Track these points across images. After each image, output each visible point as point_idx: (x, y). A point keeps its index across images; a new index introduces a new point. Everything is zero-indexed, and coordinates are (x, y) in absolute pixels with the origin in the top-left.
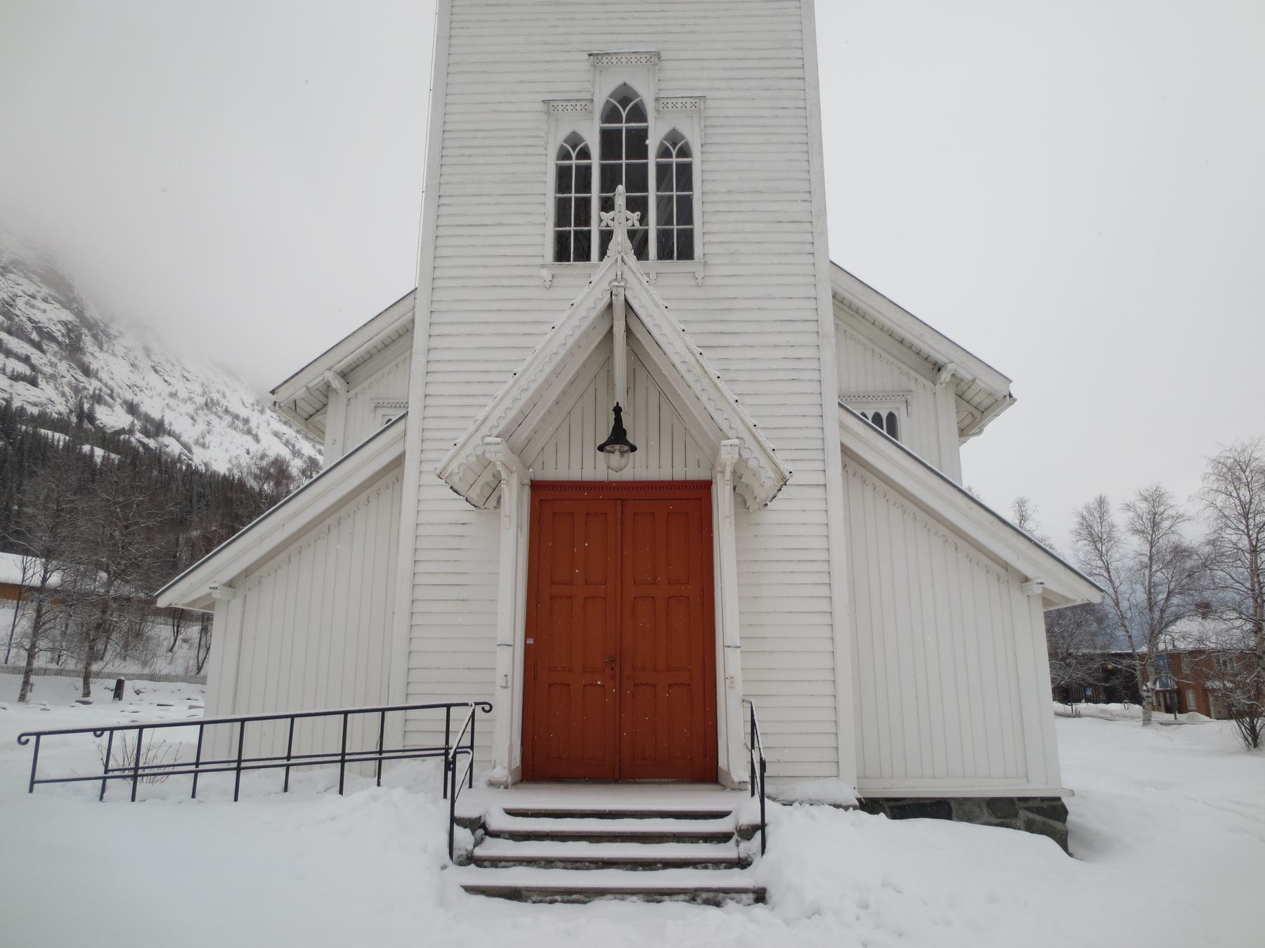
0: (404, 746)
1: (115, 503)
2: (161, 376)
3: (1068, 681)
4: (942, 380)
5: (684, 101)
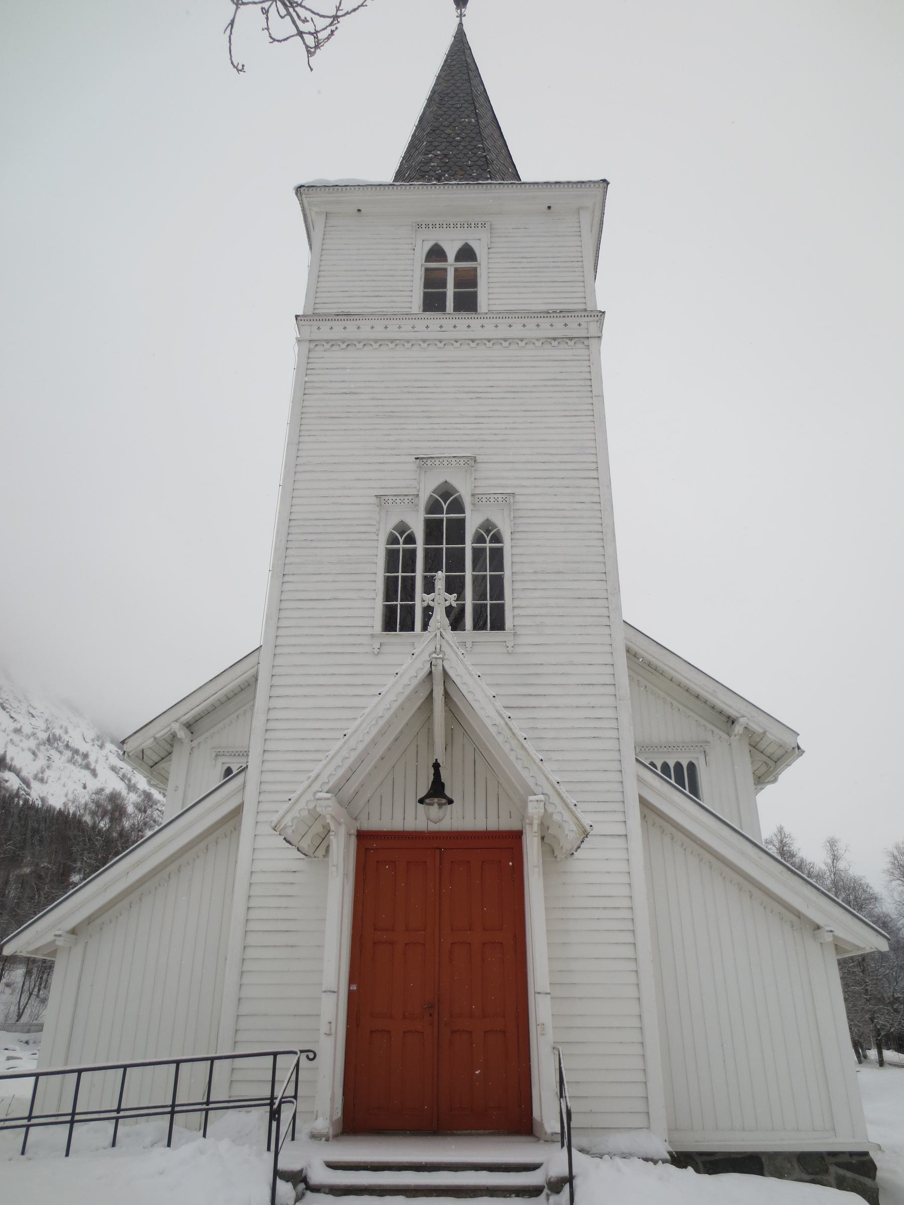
0: (230, 1097)
2: (7, 712)
3: (897, 1028)
4: (736, 732)
5: (496, 496)
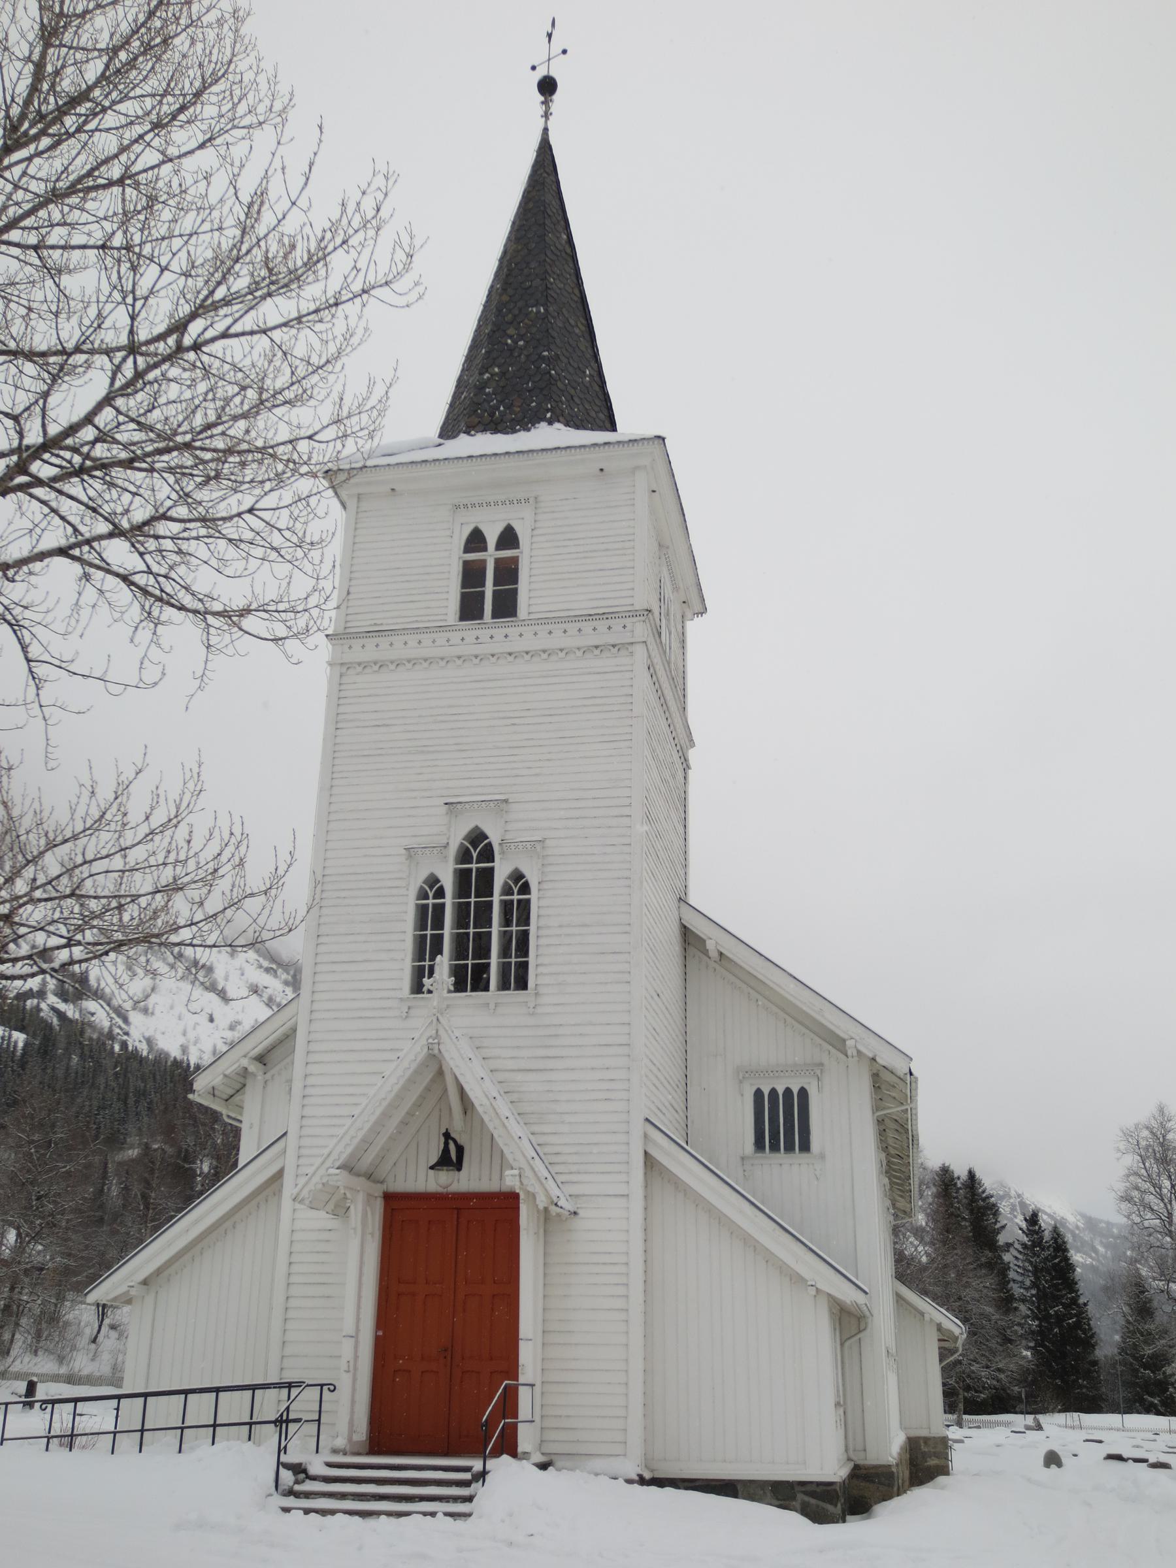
5: (524, 844)
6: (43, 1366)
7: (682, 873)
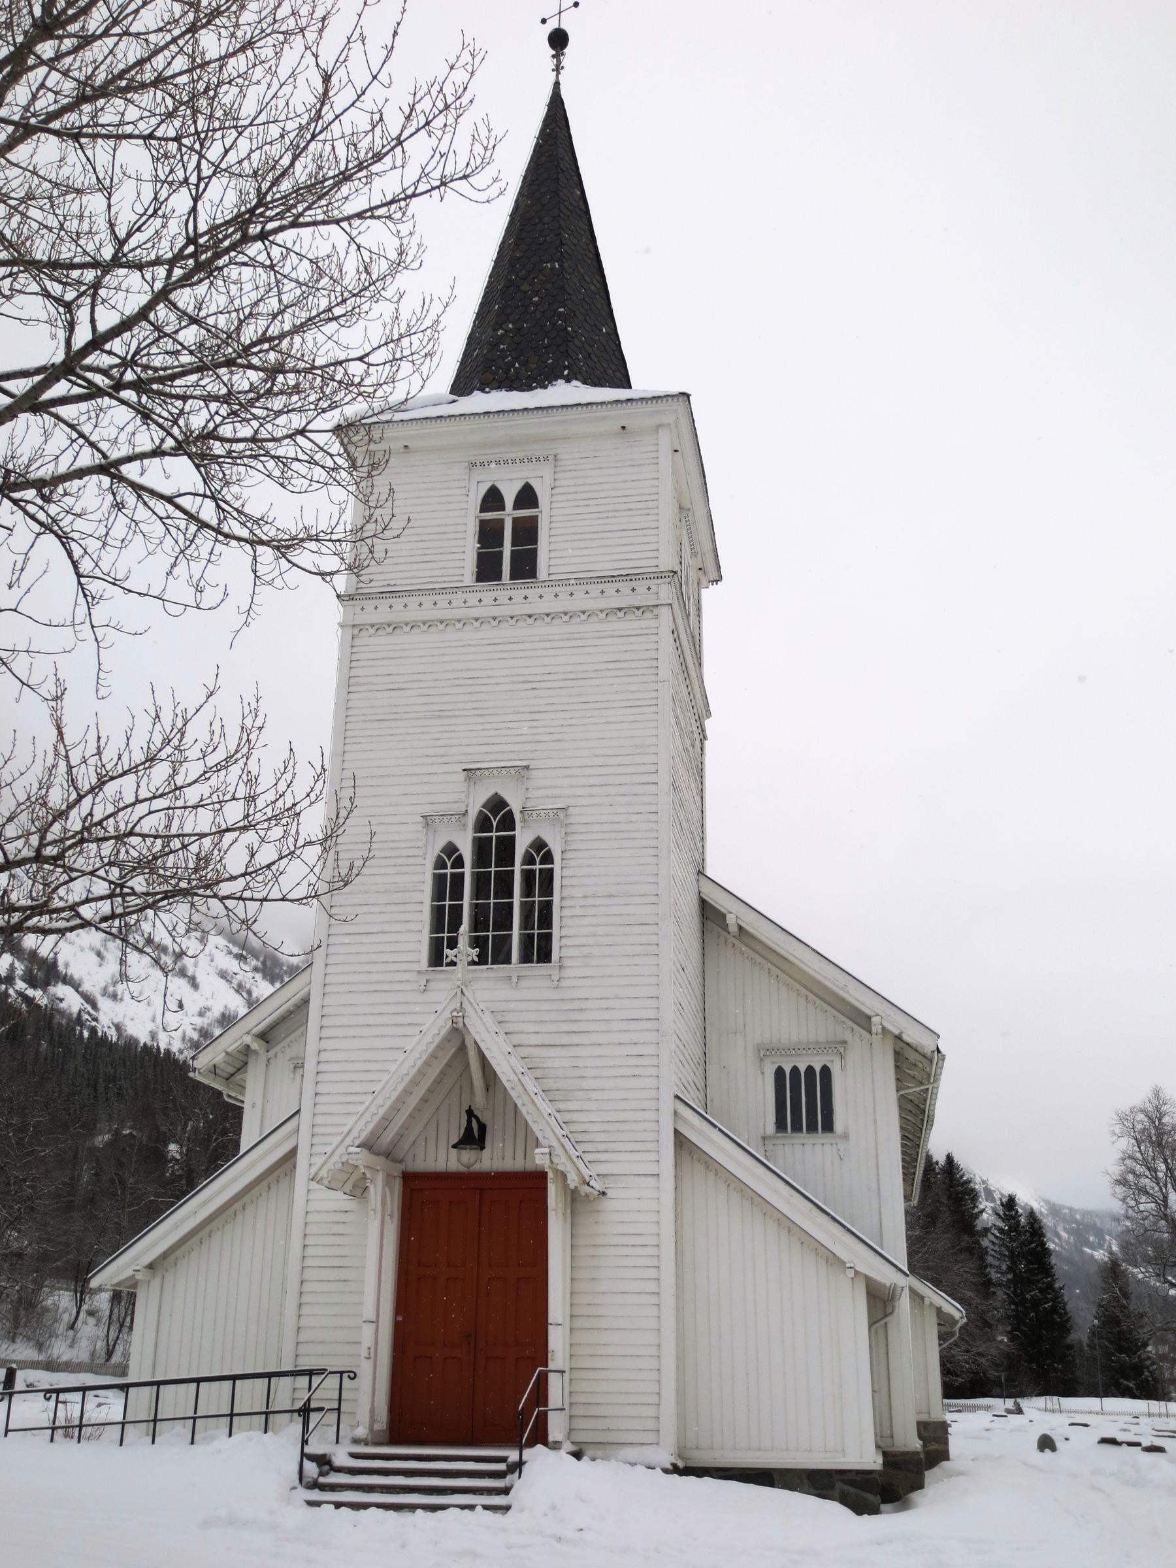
1: (8, 1126)
5: (547, 812)
6: (21, 1353)
7: (699, 845)
